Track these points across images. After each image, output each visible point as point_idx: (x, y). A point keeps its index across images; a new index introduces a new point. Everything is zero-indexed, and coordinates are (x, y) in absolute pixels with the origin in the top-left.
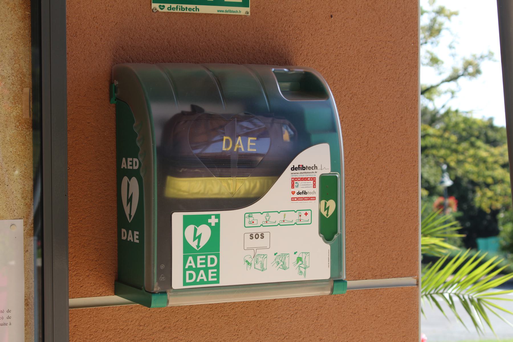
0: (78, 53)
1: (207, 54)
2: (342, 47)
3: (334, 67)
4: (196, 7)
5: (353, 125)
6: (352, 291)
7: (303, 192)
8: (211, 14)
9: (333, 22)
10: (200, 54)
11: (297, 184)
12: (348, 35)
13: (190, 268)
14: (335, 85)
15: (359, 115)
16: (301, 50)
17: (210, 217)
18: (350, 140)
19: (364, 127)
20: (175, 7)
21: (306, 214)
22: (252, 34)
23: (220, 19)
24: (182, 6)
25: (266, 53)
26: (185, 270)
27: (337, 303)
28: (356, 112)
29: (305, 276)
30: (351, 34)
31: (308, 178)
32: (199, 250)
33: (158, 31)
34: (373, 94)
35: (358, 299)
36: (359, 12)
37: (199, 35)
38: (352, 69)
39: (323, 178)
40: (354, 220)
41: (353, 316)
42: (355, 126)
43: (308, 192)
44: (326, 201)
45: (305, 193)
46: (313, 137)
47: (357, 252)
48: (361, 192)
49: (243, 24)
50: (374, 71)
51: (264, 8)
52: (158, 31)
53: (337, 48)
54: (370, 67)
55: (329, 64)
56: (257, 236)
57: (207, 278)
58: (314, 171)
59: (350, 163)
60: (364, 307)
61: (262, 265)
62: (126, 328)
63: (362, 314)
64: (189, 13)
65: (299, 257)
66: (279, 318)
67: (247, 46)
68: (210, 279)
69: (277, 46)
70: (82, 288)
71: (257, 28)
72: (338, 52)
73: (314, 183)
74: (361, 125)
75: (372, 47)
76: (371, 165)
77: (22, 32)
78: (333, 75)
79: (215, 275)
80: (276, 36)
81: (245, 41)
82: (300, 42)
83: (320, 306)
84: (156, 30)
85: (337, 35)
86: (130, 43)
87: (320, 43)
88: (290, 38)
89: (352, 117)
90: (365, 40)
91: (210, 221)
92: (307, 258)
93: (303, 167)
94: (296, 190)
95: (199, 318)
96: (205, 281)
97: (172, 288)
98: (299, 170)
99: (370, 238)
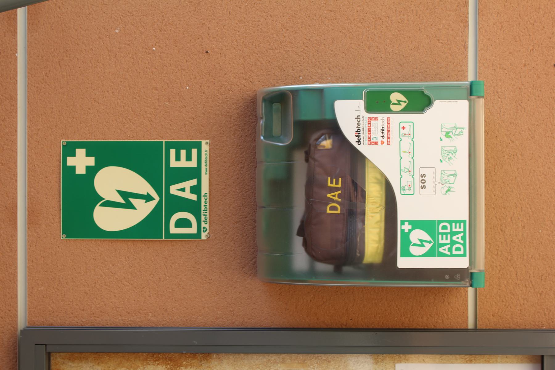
0: (249, 309)
1: (247, 184)
2: (237, 40)
3: (256, 48)
4: (203, 196)
5: (314, 28)
6: (479, 29)
7: (382, 132)
8: (210, 180)
9: (212, 51)
10: (247, 192)
11: (374, 138)
12: (225, 33)
13: (450, 250)
14: (274, 48)
15: (304, 20)
16: (240, 86)
17: (403, 231)
18: (328, 31)
19: (315, 16)
20: (204, 216)
21: (403, 128)
22: (227, 138)
23: (213, 171)
24: (203, 210)
25: (245, 124)
26: (452, 255)
27: (490, 47)
28: (301, 24)
29: (464, 128)
30: (224, 30)
31: (368, 127)
32: (433, 240)
33: (227, 234)
34: (283, 4)
35: (488, 23)
36: (202, 20)
37: (229, 192)
38: (258, 29)
39: (369, 109)
40: (408, 27)
41: (505, 29)
42: (314, 26)
43: (382, 126)
44: (392, 103)
45: (383, 129)
46: (328, 117)
47: (440, 24)
48: (381, 19)
49: (218, 147)
50: (259, 3)
51: (202, 125)
52: (227, 234)
53: (238, 46)
54: (256, 8)
55: (254, 55)
56: (423, 181)
57: (460, 232)
58: (361, 119)
59: (351, 31)
60: (496, 16)
61: (451, 175)
62: (499, 267)
63: (502, 18)
64: (209, 202)
65: (445, 136)
66: (500, 111)
67: (238, 144)
68: (462, 230)
69: (238, 111)
70: (459, 309)
71: (220, 133)
72: (241, 45)
73: (373, 119)
74: (313, 19)
75: (236, 6)
76: (354, 7)
77: (232, 362)
78: (264, 50)
79: (458, 224)
80: (228, 112)
81: (233, 146)
82: (233, 86)
83: (491, 66)
84: (226, 235)
85: (225, 46)
86: (238, 261)
87: (233, 65)
88: (229, 98)
89: (306, 29)
90: (228, 14)
91: (406, 231)
92: (446, 126)
93: (358, 132)
94: (380, 139)
95: (495, 196)
96: (463, 235)
97: (468, 268)
98: (360, 136)
99: (427, 9)
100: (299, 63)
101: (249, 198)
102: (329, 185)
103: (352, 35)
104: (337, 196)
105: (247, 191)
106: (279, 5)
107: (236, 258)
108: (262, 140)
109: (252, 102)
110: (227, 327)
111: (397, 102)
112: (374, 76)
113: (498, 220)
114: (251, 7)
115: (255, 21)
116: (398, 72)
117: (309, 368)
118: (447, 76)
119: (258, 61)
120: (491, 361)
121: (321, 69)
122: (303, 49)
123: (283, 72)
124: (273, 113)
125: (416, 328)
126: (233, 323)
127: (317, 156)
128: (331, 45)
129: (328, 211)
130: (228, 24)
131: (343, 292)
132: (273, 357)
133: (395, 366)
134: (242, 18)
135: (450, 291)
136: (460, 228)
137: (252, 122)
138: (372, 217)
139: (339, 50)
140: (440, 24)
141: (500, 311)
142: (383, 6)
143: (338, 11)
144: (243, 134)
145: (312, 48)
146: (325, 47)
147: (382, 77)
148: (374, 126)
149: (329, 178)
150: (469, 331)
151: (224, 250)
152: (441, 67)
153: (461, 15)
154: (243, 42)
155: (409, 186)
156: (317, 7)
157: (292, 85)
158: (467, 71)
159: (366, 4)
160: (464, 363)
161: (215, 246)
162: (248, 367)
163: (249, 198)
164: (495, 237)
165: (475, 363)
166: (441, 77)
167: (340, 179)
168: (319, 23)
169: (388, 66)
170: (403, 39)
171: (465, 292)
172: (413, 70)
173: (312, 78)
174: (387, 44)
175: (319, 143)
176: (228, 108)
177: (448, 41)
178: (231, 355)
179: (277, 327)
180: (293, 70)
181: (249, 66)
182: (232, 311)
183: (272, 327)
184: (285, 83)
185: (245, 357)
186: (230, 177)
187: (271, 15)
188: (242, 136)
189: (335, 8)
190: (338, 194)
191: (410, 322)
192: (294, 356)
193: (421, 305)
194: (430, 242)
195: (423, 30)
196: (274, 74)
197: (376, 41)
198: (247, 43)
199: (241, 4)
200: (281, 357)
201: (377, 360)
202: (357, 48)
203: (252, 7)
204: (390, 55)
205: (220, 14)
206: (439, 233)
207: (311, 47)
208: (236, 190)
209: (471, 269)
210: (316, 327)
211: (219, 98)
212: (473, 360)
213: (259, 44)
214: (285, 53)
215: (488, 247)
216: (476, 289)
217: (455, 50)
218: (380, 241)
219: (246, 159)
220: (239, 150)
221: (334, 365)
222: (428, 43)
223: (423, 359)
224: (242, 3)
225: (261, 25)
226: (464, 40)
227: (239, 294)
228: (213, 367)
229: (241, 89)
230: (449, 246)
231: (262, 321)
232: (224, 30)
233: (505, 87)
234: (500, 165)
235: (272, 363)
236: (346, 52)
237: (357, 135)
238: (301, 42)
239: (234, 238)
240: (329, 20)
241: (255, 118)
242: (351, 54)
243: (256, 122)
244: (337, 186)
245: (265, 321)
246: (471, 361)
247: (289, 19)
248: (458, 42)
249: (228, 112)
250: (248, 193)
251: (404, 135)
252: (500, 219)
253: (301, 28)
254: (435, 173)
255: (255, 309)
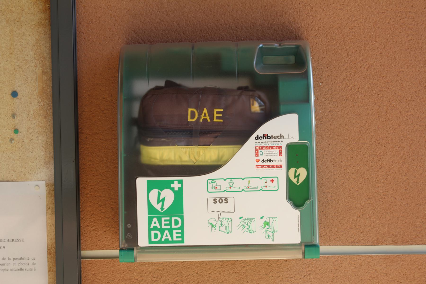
0: (94, 38)
1: (216, 33)
3: (349, 40)
6: (371, 256)
10: (208, 33)
11: (262, 153)
12: (363, 8)
13: (155, 228)
14: (349, 57)
17: (173, 182)
21: (272, 181)
22: (261, 12)
25: (275, 30)
26: (150, 230)
28: (374, 83)
30: (366, 7)
31: (273, 147)
37: (207, 16)
38: (368, 41)
39: (290, 147)
40: (372, 187)
41: (371, 281)
42: (372, 96)
46: (282, 108)
47: (375, 218)
48: (379, 160)
55: (343, 37)
56: (221, 201)
58: (280, 140)
60: (384, 272)
61: (227, 228)
65: (265, 222)
66: (291, 278)
68: (175, 239)
73: (281, 151)
74: (379, 94)
75: (391, 19)
78: (347, 47)
79: (180, 235)
81: (253, 19)
82: (311, 17)
84: (166, 14)
85: (351, 9)
86: (141, 27)
87: (333, 17)
88: (300, 14)
89: (369, 88)
90: (382, 12)
91: (172, 186)
93: (268, 137)
94: (261, 158)
95: (210, 274)
97: (138, 246)
98: (264, 139)
100: (335, 82)
101: (202, 36)
102: (216, 110)
103: (364, 133)
104: (205, 118)
105: (210, 33)
106: (392, 61)
107: (143, 24)
108: (259, 45)
109: (296, 37)
110: (76, 18)
111: (297, 174)
112: (324, 155)
113: (186, 278)
114: (389, 33)
115: (375, 38)
116: (328, 178)
117: (38, 98)
118: (325, 225)
119: (336, 41)
120: (50, 273)
121: (329, 103)
122: (348, 85)
123: (326, 66)
124: (285, 56)
125: (80, 201)
126: (80, 23)
127: (244, 98)
128: (353, 113)
129: (190, 110)
130: (373, 11)
131: (113, 129)
132: (48, 63)
133: (43, 181)
134: (379, 25)
135: (116, 232)
136: (177, 237)
137: (276, 37)
138: (186, 153)
139: (349, 121)
140: (375, 218)
141: (98, 281)
142: (392, 162)
143: (387, 119)
144: (264, 28)
145: (350, 94)
146: (351, 106)
147: (323, 163)
148: (273, 152)
149: (222, 110)
150: (79, 252)
151: (151, 12)
152: (334, 219)
153: (384, 238)
154: (355, 26)
155: (216, 188)
156: (391, 99)
157: (313, 75)
158: (330, 245)
159: (394, 146)
160: (48, 247)
161: (155, 4)
162: (38, 39)
163: (202, 36)
164: (170, 274)
165: (48, 257)
166: (324, 220)
167: (222, 121)
168: (375, 100)
169: (334, 169)
170: (360, 183)
171: (116, 247)
172: (330, 192)
173: (320, 95)
174: (355, 167)
175: (256, 99)
176: (290, 13)
177: (359, 226)
178: (49, 21)
179: (78, 66)
180: (328, 76)
181: (331, 33)
182: (92, 22)
183: (78, 61)
184: (315, 68)
185: (48, 36)
186: (223, 16)
187: (382, 53)
188: (263, 27)
189: (390, 116)
190: (206, 119)
191: (86, 194)
192: (50, 83)
193: (102, 204)
194: (162, 209)
195: (368, 202)
196: (324, 57)
197: (358, 156)
198: (354, 31)
199: (392, 24)
200: (49, 70)
201: (49, 164)
202: (351, 138)
203: (390, 34)
204: (344, 170)
205: (383, 3)
206: (171, 218)
207: (351, 93)
208: (210, 23)
209: (137, 249)
210: (79, 104)
211: (299, 4)
212: (51, 256)
213: (353, 42)
214: (345, 68)
215: (160, 268)
216: (118, 257)
217: (350, 233)
218: (162, 160)
219: (240, 32)
220: (249, 25)
221: (42, 121)
222: (357, 207)
223: (50, 207)
224: (393, 24)
225: (372, 43)
226: (360, 241)
227: (109, 28)
228: (37, 4)
229: (309, 25)
230: (159, 227)
231: (83, 51)
232: (366, 7)
233: (315, 282)
234: (239, 278)
235: (43, 61)
236: (347, 127)
237: (265, 136)
238: (356, 83)
239: (163, 22)
240: (378, 110)
241: (280, 39)
242: (345, 133)
243: (276, 40)
244: (215, 118)
245: (84, 54)
246: (49, 254)
247: (379, 71)
248: (358, 236)
249: (286, 14)
250: (207, 34)
251: (266, 181)
252: (187, 279)
253: (369, 83)
254: (230, 212)
255: (95, 44)
